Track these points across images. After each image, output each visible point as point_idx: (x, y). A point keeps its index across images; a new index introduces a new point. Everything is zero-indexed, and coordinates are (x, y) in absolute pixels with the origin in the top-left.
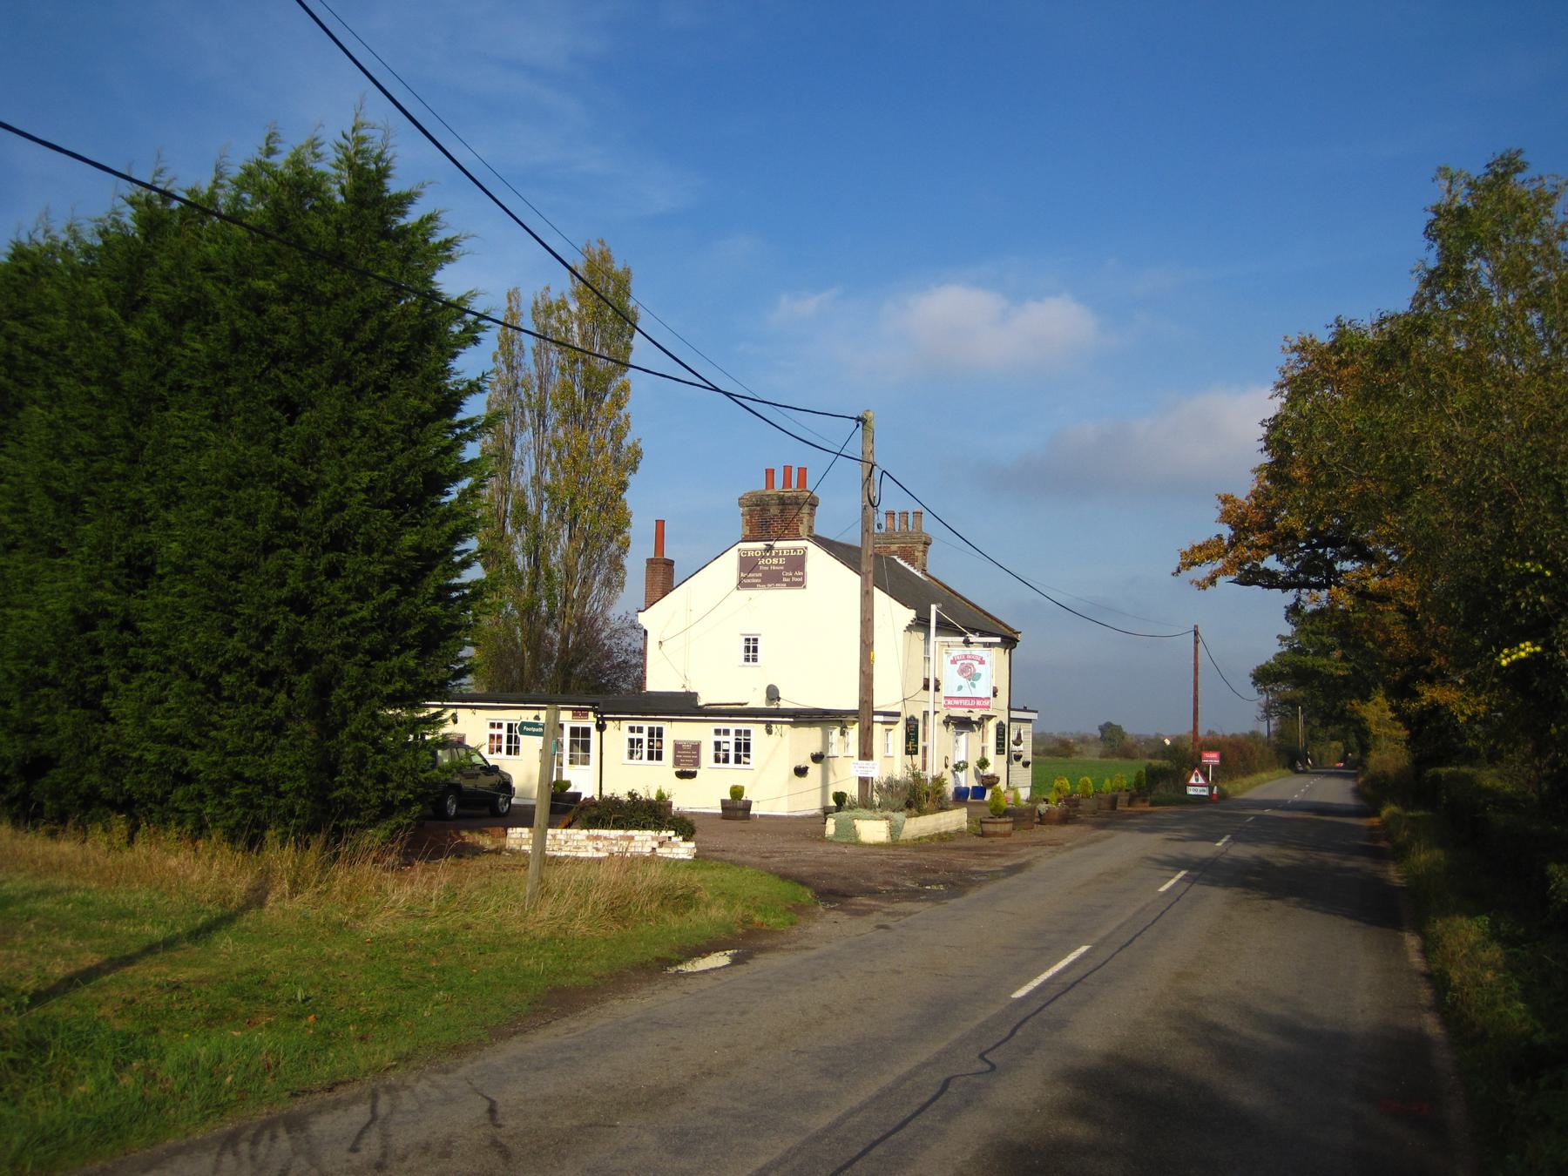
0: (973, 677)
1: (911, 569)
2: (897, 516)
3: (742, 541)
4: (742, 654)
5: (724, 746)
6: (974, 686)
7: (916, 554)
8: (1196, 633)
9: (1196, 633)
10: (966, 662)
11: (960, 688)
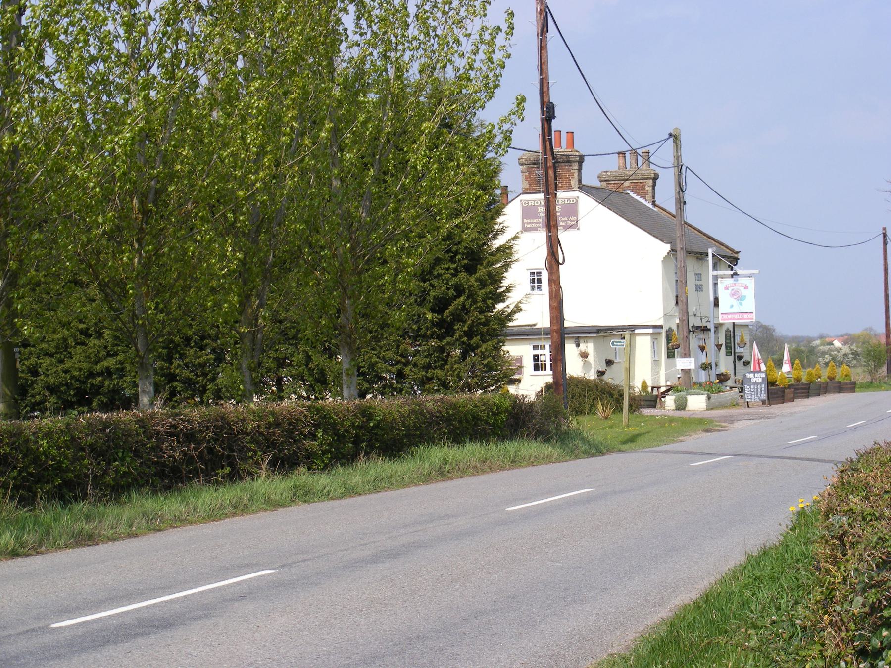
0: (740, 298)
1: (643, 201)
2: (628, 155)
3: (523, 194)
4: (529, 285)
5: (542, 358)
6: (741, 304)
7: (647, 188)
8: (885, 235)
9: (885, 235)
10: (735, 288)
11: (732, 306)
